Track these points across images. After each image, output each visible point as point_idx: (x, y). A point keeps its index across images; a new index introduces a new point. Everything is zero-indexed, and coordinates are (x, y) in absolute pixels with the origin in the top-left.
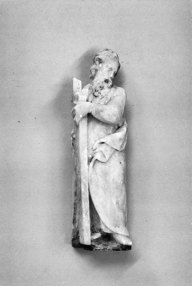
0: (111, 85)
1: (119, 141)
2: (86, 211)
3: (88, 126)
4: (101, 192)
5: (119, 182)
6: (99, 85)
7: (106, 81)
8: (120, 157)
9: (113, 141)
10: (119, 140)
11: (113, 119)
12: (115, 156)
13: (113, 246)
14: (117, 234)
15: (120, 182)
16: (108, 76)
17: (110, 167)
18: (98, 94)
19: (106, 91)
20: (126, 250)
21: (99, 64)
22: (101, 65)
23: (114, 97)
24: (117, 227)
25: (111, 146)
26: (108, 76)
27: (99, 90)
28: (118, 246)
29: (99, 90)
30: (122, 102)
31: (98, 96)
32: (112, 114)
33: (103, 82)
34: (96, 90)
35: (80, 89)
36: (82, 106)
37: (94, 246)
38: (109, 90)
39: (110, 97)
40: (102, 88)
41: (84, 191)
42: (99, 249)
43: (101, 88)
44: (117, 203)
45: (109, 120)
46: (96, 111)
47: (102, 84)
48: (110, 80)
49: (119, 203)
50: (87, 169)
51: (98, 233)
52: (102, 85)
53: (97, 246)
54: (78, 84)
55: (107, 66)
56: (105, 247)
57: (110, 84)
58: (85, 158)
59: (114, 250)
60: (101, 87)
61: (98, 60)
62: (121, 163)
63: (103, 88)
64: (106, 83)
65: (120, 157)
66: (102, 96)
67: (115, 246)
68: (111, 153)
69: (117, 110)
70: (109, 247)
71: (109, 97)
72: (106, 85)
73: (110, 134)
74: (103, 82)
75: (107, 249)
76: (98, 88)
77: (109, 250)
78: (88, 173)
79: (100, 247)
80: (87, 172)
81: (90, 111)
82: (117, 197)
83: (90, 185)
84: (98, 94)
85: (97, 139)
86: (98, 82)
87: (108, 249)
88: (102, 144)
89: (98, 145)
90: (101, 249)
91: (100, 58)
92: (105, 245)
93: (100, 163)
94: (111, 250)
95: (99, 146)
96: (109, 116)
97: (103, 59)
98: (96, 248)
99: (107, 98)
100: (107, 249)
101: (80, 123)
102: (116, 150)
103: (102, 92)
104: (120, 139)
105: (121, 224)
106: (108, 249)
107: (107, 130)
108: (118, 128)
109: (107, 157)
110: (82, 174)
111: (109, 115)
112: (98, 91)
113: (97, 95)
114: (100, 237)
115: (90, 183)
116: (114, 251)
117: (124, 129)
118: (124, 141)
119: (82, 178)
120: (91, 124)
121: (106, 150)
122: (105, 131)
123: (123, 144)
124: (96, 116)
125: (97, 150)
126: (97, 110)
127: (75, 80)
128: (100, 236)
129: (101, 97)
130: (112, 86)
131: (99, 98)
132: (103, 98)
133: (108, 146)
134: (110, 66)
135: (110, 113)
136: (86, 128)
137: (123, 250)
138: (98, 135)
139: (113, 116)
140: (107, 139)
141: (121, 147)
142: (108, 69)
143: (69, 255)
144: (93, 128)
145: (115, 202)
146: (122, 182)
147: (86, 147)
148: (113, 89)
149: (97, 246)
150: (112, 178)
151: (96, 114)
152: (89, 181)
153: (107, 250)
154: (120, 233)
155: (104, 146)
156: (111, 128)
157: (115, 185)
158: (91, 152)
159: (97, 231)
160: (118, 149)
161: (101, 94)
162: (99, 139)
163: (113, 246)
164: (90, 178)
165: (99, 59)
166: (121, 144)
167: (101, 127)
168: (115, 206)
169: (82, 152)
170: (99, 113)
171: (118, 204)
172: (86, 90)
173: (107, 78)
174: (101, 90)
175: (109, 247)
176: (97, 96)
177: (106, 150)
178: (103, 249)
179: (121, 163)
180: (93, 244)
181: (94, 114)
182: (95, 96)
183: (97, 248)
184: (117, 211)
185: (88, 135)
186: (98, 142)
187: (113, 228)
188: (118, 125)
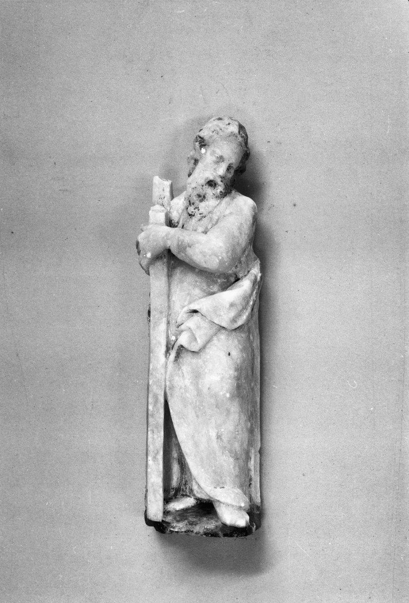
0: (221, 192)
1: (229, 309)
2: (156, 452)
3: (170, 276)
4: (191, 414)
5: (221, 393)
6: (195, 193)
7: (211, 184)
8: (230, 342)
9: (216, 310)
10: (228, 306)
11: (213, 264)
12: (219, 340)
13: (206, 527)
14: (218, 501)
15: (224, 395)
16: (214, 174)
17: (204, 362)
18: (195, 209)
19: (211, 202)
20: (234, 536)
21: (201, 149)
22: (203, 151)
23: (224, 216)
24: (218, 488)
25: (209, 319)
26: (214, 174)
27: (197, 202)
28: (217, 527)
29: (197, 202)
30: (239, 229)
31: (193, 214)
32: (210, 252)
33: (203, 186)
34: (192, 202)
35: (165, 199)
36: (150, 235)
37: (168, 523)
38: (217, 203)
39: (217, 218)
40: (202, 198)
41: (153, 409)
42: (176, 530)
43: (200, 198)
44: (219, 437)
45: (205, 265)
46: (178, 245)
47: (201, 190)
48: (219, 181)
49: (223, 437)
50: (163, 365)
51: (189, 498)
52: (202, 193)
53: (175, 525)
54: (161, 190)
55: (214, 152)
56: (190, 527)
57: (220, 189)
58: (159, 343)
59: (206, 534)
60: (199, 196)
61: (200, 139)
62: (229, 354)
63: (204, 197)
64: (213, 188)
65: (230, 342)
66: (202, 215)
67: (211, 525)
68: (211, 332)
69: (221, 244)
70: (198, 529)
71: (215, 217)
72: (209, 191)
73: (213, 293)
74: (203, 186)
75: (192, 531)
76: (195, 199)
77: (196, 533)
78: (166, 372)
79: (180, 527)
80: (163, 371)
81: (169, 244)
82: (218, 426)
83: (169, 398)
84: (195, 209)
85: (186, 303)
86: (193, 185)
87: (195, 531)
88: (194, 314)
89: (185, 316)
90: (182, 532)
91: (202, 136)
92: (191, 524)
93: (190, 354)
94: (202, 535)
95: (188, 318)
96: (205, 256)
97: (206, 138)
98: (172, 529)
99: (211, 218)
100: (192, 531)
101: (150, 268)
102: (221, 326)
103: (202, 205)
104: (232, 305)
105: (228, 481)
106: (195, 531)
107: (209, 286)
108: (229, 280)
109: (200, 342)
110: (152, 374)
111: (203, 254)
112: (193, 204)
113: (192, 212)
114: (193, 507)
115: (168, 394)
116: (206, 536)
117: (245, 285)
118: (244, 308)
119: (150, 384)
120: (178, 274)
121: (199, 327)
122: (205, 288)
123: (239, 315)
124: (180, 256)
125: (183, 327)
126: (180, 243)
127: (157, 180)
128: (193, 505)
129: (198, 216)
130: (223, 195)
131: (196, 219)
132: (204, 219)
133: (205, 318)
134: (219, 152)
135: (206, 250)
136: (164, 279)
137: (225, 535)
138: (189, 294)
139: (213, 257)
140: (204, 304)
141: (234, 320)
142: (214, 159)
143: (147, 537)
144: (181, 281)
145: (213, 434)
146: (228, 395)
147: (164, 320)
148: (227, 199)
149: (175, 525)
150: (208, 386)
151: (179, 253)
152: (167, 388)
153: (193, 534)
154: (222, 500)
155: (196, 317)
156: (219, 281)
157: (213, 401)
158: (173, 329)
159: (188, 494)
160: (224, 324)
161: (199, 210)
162: (190, 303)
163: (206, 527)
164: (168, 383)
165: (200, 137)
166: (232, 314)
167: (197, 279)
168: (215, 444)
169: (154, 330)
170: (185, 249)
171: (221, 439)
172: (178, 201)
173: (211, 178)
174: (201, 201)
175: (198, 529)
176: (192, 215)
177: (199, 327)
178: (185, 532)
179: (229, 354)
180: (169, 519)
181: (174, 251)
182: (190, 215)
183: (174, 528)
184: (219, 453)
185: (169, 296)
186: (186, 309)
187: (210, 488)
188: (236, 276)
